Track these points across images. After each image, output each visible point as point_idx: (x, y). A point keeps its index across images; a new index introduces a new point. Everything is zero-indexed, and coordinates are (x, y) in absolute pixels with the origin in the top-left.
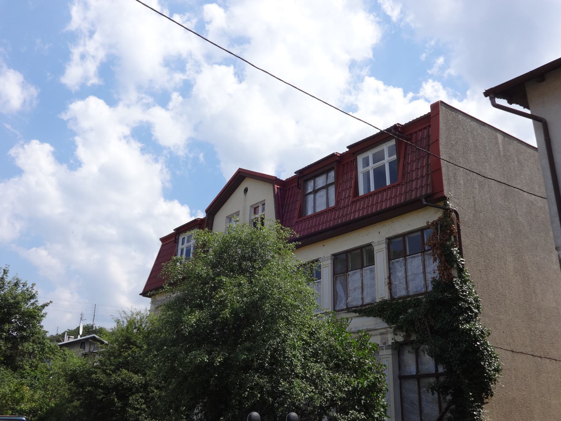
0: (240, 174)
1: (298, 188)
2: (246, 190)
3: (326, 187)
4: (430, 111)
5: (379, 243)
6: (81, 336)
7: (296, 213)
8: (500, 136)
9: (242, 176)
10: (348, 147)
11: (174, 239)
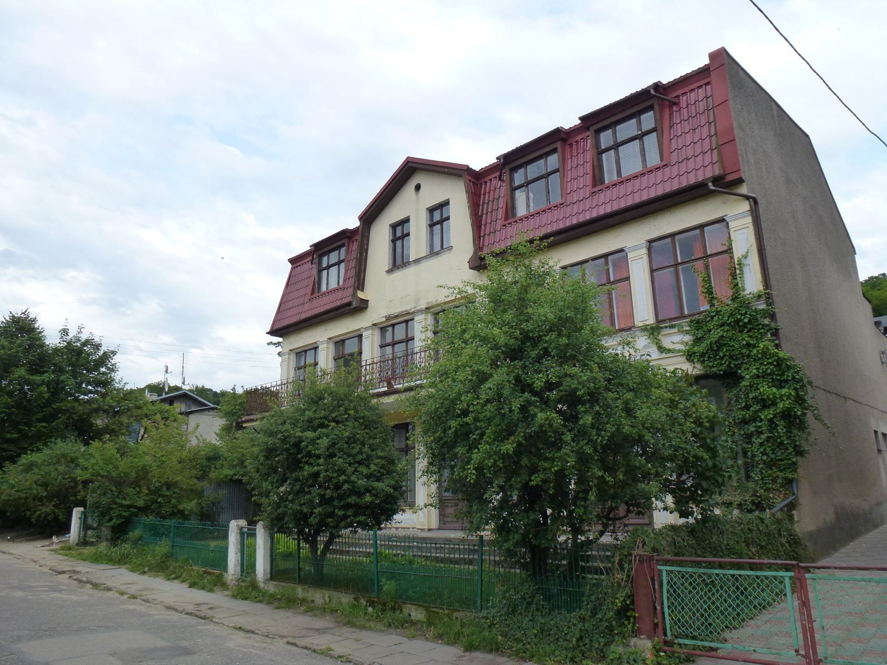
0: (410, 164)
1: (500, 179)
2: (418, 188)
3: (338, 263)
4: (708, 62)
5: (636, 248)
6: (166, 393)
7: (501, 213)
8: (774, 107)
9: (411, 170)
10: (580, 119)
11: (311, 258)
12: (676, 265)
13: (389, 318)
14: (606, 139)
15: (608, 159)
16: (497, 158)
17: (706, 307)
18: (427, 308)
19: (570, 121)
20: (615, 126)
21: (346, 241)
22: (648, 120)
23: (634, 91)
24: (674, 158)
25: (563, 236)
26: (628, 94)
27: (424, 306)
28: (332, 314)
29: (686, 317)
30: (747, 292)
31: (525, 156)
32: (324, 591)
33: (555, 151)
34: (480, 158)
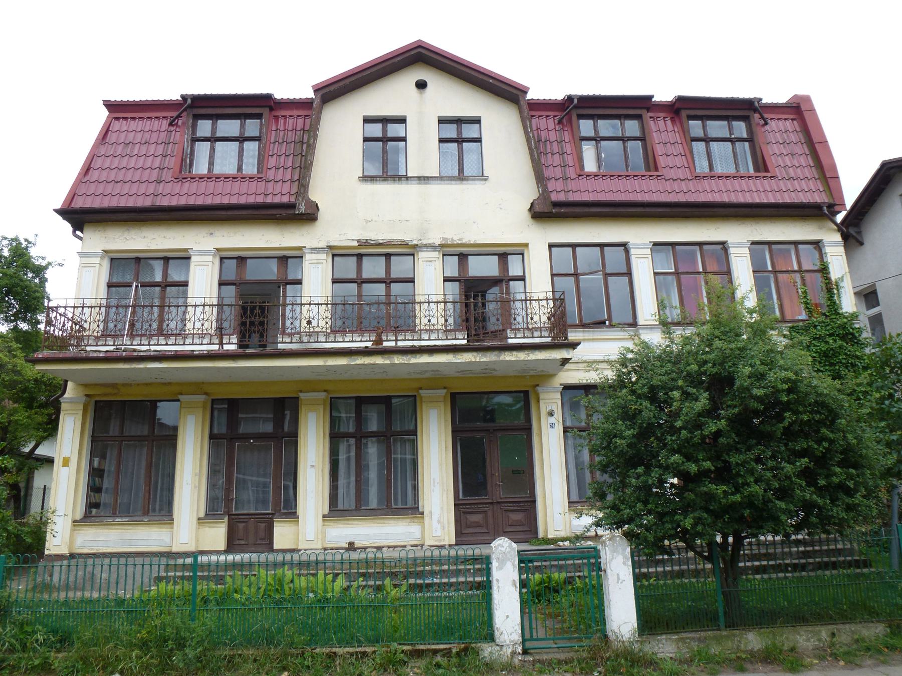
2: (421, 85)
5: (739, 245)
9: (419, 57)
11: (175, 114)
12: (576, 275)
13: (364, 243)
14: (204, 127)
15: (203, 149)
16: (182, 96)
17: (804, 316)
18: (442, 246)
19: (664, 94)
20: (245, 119)
21: (265, 112)
22: (252, 127)
23: (597, 93)
24: (271, 174)
25: (668, 210)
26: (591, 93)
27: (438, 242)
28: (244, 212)
29: (786, 322)
30: (844, 311)
31: (608, 107)
32: (817, 628)
33: (259, 116)
34: (544, 88)
